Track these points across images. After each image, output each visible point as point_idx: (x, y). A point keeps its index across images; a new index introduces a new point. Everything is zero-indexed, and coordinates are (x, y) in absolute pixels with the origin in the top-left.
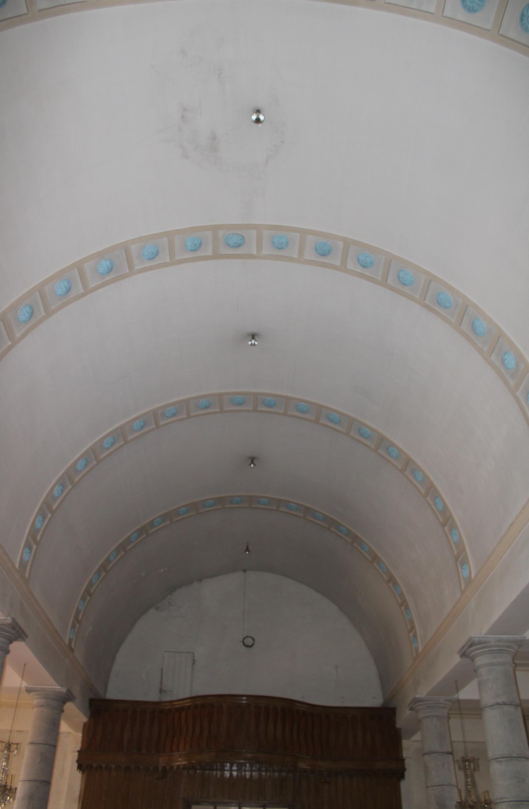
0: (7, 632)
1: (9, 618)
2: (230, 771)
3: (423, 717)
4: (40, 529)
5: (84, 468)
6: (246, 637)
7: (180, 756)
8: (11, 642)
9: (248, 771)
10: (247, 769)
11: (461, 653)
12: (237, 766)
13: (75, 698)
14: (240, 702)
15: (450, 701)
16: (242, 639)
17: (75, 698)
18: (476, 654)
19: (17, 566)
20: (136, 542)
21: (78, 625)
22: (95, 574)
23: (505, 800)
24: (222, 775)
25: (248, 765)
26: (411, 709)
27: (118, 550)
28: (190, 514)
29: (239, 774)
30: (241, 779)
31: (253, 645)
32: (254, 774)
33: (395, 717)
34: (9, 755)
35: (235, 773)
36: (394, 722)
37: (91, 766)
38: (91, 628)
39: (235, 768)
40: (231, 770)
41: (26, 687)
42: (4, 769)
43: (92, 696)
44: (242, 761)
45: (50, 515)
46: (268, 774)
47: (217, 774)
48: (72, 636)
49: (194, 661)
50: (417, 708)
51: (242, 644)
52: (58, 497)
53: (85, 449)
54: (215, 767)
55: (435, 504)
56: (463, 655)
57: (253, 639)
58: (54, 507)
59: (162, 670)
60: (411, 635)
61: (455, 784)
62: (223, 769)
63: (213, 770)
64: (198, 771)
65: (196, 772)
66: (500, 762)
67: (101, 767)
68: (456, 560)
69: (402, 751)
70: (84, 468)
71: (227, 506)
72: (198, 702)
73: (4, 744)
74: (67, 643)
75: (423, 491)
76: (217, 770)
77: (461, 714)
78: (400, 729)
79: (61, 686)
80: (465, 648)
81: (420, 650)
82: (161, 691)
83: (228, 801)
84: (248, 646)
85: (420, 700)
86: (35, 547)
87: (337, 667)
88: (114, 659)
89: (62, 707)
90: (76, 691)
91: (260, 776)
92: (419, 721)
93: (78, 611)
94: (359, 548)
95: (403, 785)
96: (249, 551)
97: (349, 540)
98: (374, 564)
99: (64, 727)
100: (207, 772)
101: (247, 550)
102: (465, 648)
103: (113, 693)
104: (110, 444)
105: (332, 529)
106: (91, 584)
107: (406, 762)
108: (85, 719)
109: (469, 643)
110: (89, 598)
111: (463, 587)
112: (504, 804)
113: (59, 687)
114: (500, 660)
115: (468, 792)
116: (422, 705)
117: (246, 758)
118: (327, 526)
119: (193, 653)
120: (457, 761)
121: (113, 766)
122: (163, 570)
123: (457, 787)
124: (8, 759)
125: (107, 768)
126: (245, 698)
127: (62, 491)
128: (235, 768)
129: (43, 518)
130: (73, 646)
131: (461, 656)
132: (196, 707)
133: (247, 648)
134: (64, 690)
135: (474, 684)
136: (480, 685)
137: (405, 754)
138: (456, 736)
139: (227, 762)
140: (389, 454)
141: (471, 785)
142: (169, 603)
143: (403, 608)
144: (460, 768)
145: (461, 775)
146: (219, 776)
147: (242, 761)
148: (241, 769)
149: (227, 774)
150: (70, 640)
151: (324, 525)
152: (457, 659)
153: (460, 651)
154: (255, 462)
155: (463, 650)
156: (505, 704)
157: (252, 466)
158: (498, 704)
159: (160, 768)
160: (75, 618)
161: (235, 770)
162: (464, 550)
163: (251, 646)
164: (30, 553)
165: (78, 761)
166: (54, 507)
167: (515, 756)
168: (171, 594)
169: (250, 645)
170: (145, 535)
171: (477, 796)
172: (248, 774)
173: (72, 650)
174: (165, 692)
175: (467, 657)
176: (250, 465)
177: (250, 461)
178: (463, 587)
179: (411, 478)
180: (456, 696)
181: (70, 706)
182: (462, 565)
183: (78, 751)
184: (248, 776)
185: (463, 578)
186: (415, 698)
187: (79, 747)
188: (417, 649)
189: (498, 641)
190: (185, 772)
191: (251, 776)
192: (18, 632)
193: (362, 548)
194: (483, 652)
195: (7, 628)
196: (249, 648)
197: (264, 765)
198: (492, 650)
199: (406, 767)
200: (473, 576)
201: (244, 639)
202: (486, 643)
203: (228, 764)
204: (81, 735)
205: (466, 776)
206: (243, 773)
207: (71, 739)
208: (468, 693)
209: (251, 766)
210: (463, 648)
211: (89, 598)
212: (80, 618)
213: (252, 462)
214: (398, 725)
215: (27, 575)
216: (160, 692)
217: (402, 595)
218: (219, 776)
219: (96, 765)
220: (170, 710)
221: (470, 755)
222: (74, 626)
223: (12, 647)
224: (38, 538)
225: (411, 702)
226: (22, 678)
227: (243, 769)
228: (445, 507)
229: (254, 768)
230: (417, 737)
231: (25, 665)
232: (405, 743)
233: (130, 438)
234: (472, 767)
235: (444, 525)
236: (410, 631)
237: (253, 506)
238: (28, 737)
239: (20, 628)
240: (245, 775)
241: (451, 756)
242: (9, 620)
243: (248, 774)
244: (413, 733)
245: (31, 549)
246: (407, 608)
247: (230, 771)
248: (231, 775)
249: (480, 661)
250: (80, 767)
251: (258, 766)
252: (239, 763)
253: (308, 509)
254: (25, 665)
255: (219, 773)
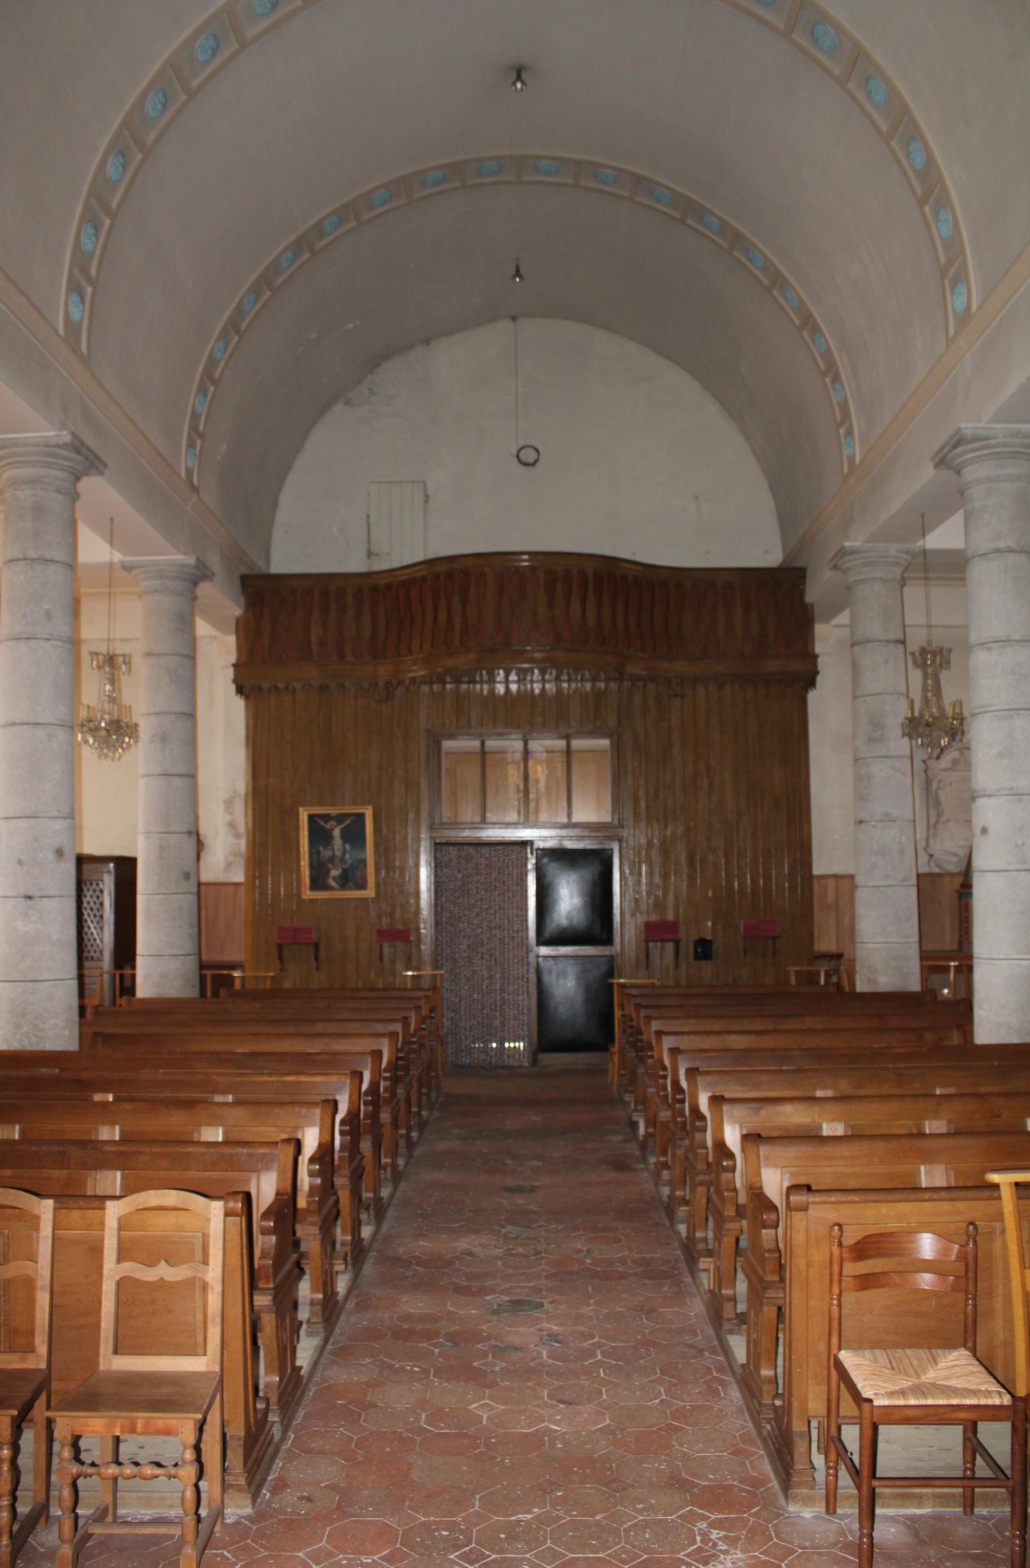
0: (65, 459)
1: (65, 433)
2: (505, 683)
3: (856, 581)
4: (93, 252)
5: (163, 112)
6: (523, 448)
7: (415, 662)
8: (78, 479)
9: (537, 682)
10: (535, 678)
11: (937, 459)
12: (518, 674)
13: (213, 574)
14: (517, 564)
15: (908, 552)
16: (515, 453)
17: (213, 574)
18: (966, 460)
19: (61, 332)
20: (292, 269)
21: (199, 442)
22: (217, 340)
23: (990, 709)
24: (492, 691)
25: (536, 671)
26: (836, 567)
27: (256, 290)
28: (395, 204)
29: (522, 688)
30: (525, 698)
31: (536, 461)
32: (548, 686)
33: (804, 583)
34: (113, 675)
35: (514, 687)
36: (802, 593)
37: (260, 687)
38: (225, 446)
39: (513, 677)
40: (507, 681)
41: (121, 562)
42: (109, 696)
43: (244, 570)
44: (526, 665)
45: (108, 222)
46: (573, 685)
47: (482, 689)
48: (190, 464)
49: (427, 496)
50: (849, 564)
51: (516, 460)
52: (118, 181)
53: (158, 66)
54: (478, 678)
55: (908, 155)
56: (941, 461)
57: (537, 451)
58: (114, 204)
59: (368, 516)
60: (842, 431)
61: (904, 691)
62: (492, 681)
63: (474, 682)
64: (448, 686)
65: (444, 688)
66: (989, 649)
67: (276, 687)
68: (943, 275)
69: (813, 641)
70: (163, 112)
71: (470, 182)
72: (440, 568)
73: (101, 658)
74: (183, 475)
75: (884, 128)
76: (481, 682)
77: (926, 578)
78: (812, 605)
79: (185, 554)
80: (946, 450)
81: (858, 460)
82: (370, 554)
83: (506, 730)
84: (527, 464)
85: (853, 552)
86: (89, 290)
87: (697, 498)
88: (276, 503)
89: (193, 592)
90: (214, 561)
91: (559, 691)
92: (849, 588)
93: (195, 417)
94: (744, 260)
95: (813, 697)
96: (520, 276)
97: (725, 245)
98: (775, 292)
99: (203, 628)
100: (464, 686)
101: (518, 273)
102: (946, 450)
103: (286, 559)
104: (210, 51)
105: (689, 221)
106: (212, 362)
107: (820, 660)
108: (238, 612)
109: (955, 439)
110: (212, 388)
111: (952, 332)
112: (987, 715)
113: (181, 557)
114: (1011, 471)
115: (926, 701)
116: (856, 559)
117: (532, 661)
118: (678, 216)
119: (424, 483)
120: (913, 654)
121: (298, 686)
122: (351, 326)
123: (908, 696)
124: (113, 681)
125: (287, 688)
126: (526, 557)
127: (125, 167)
128: (513, 677)
129: (82, 297)
130: (195, 482)
131: (936, 466)
132: (437, 577)
133: (524, 468)
134: (191, 560)
135: (957, 519)
136: (967, 518)
137: (819, 648)
138: (914, 616)
139: (498, 669)
140: (816, 43)
141: (934, 689)
142: (370, 390)
143: (828, 380)
144: (915, 664)
145: (916, 676)
146: (485, 693)
147: (526, 665)
148: (524, 679)
149: (500, 689)
150: (189, 472)
151: (673, 213)
152: (928, 472)
153: (934, 457)
154: (524, 76)
155: (941, 455)
156: (1010, 550)
157: (519, 85)
158: (997, 550)
159: (381, 684)
160: (190, 427)
161: (514, 682)
162: (962, 253)
163: (533, 464)
164: (83, 303)
165: (235, 681)
166: (114, 204)
167: (1017, 638)
168: (371, 372)
169: (531, 461)
170: (308, 255)
171: (941, 709)
172: (537, 688)
173: (195, 489)
174: (377, 555)
175: (949, 468)
176: (514, 84)
177: (514, 76)
178: (952, 332)
179: (861, 97)
180: (920, 543)
181: (205, 589)
182: (954, 285)
183: (234, 665)
184: (537, 691)
185: (954, 312)
186: (843, 548)
187: (233, 658)
188: (851, 459)
189: (1012, 436)
190: (425, 688)
191: (543, 690)
192: (86, 458)
193: (750, 260)
194: (979, 457)
195: (65, 453)
196: (531, 468)
197: (565, 671)
198: (995, 453)
199: (820, 667)
200: (974, 306)
201: (519, 451)
202: (987, 439)
203: (501, 672)
204: (232, 639)
205: (925, 677)
206: (529, 686)
207: (218, 650)
208: (946, 536)
209: (543, 672)
210: (942, 449)
211: (212, 388)
212: (201, 428)
213: (519, 78)
214: (809, 598)
215: (84, 348)
216: (369, 557)
217: (828, 354)
218: (485, 693)
219: (268, 685)
220: (389, 587)
221: (936, 644)
222: (191, 444)
223: (81, 486)
224: (93, 272)
225: (836, 555)
226: (111, 545)
227: (529, 678)
228: (930, 161)
229: (547, 677)
230: (843, 618)
231: (112, 520)
232: (820, 629)
233: (250, 34)
234: (938, 662)
235: (922, 202)
236: (839, 426)
237: (525, 178)
238: (136, 651)
239: (89, 449)
240: (532, 690)
241: (901, 647)
242: (66, 437)
243: (537, 688)
244: (834, 611)
245: (82, 296)
246: (836, 379)
247: (505, 683)
248: (507, 689)
249: (973, 473)
250: (240, 690)
251: (554, 672)
252: (518, 669)
253: (639, 181)
254: (112, 520)
255: (486, 687)
